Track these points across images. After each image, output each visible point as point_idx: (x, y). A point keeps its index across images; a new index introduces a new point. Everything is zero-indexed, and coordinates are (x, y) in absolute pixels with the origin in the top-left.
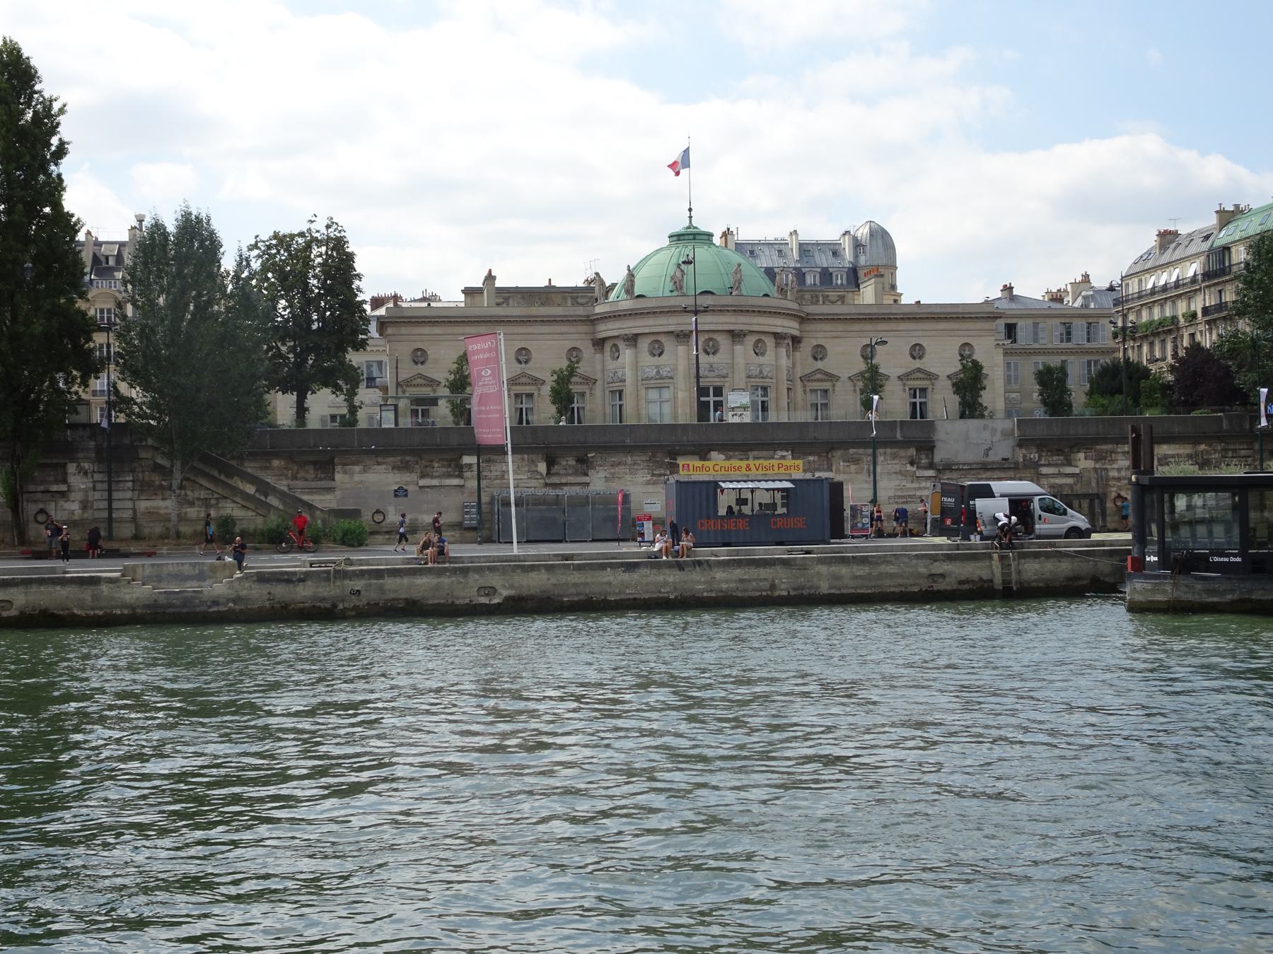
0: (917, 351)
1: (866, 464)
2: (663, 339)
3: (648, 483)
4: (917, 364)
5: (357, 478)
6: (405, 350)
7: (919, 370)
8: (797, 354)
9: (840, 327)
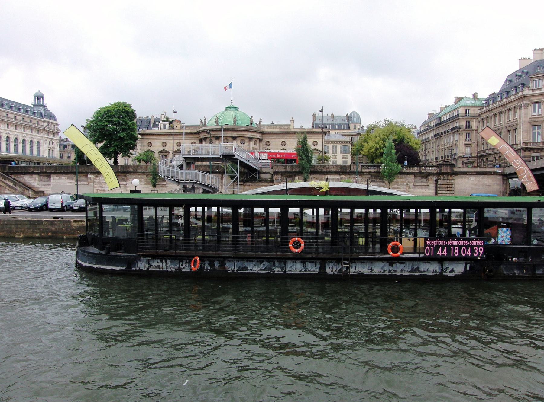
0: (164, 144)
1: (75, 178)
2: (213, 139)
3: (145, 184)
4: (164, 148)
5: (57, 181)
6: (176, 142)
7: (315, 149)
8: (261, 144)
9: (167, 137)
